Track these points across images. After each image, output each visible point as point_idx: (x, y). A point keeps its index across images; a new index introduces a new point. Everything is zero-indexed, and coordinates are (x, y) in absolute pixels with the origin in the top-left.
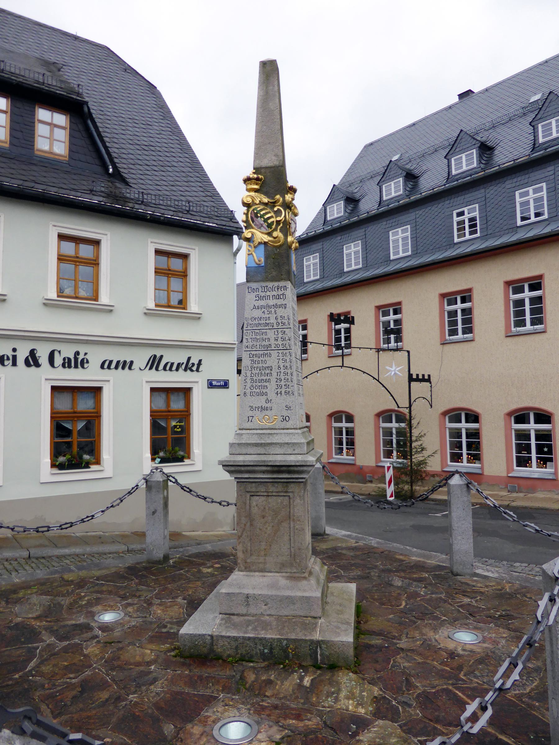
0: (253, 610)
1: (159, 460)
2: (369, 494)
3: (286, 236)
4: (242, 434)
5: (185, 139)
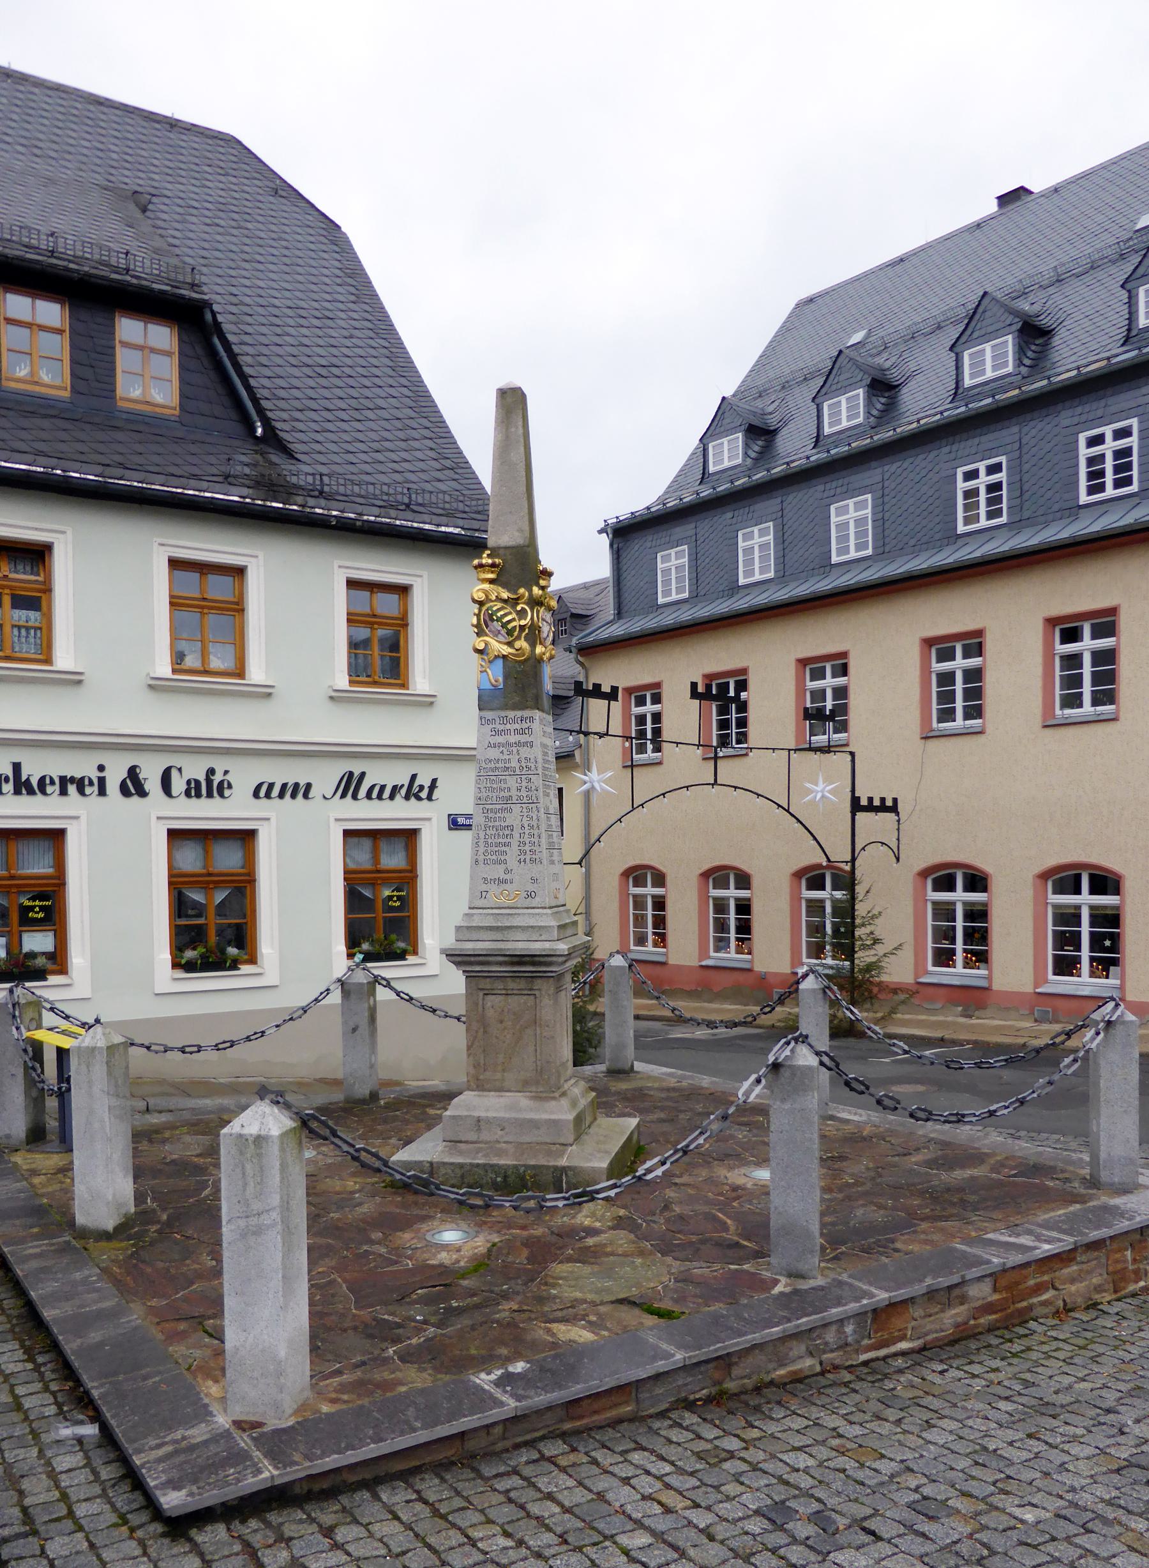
0: (485, 1136)
1: (361, 956)
2: (773, 1026)
3: (533, 646)
4: (473, 915)
5: (400, 345)
